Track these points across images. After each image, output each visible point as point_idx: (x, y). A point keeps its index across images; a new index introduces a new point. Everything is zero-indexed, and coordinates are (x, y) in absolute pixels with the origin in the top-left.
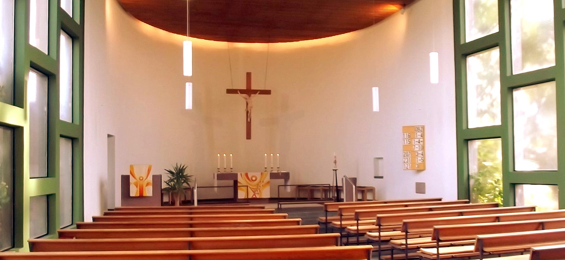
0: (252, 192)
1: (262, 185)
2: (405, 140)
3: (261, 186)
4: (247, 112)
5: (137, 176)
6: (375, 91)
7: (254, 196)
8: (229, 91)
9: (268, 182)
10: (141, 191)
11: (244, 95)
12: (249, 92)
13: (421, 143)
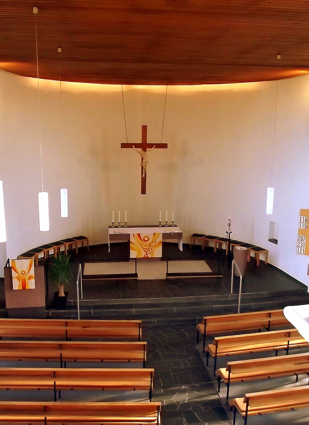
2: (302, 224)
3: (153, 246)
4: (142, 168)
6: (270, 193)
7: (146, 256)
10: (24, 285)
12: (144, 146)
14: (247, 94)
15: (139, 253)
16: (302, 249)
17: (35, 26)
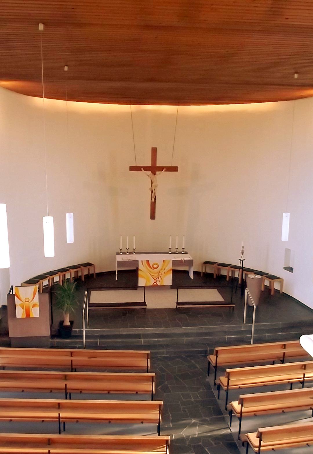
0: (154, 280)
1: (164, 273)
3: (163, 273)
4: (152, 192)
5: (22, 297)
6: (286, 219)
7: (155, 284)
8: (133, 169)
12: (154, 169)
15: (148, 280)
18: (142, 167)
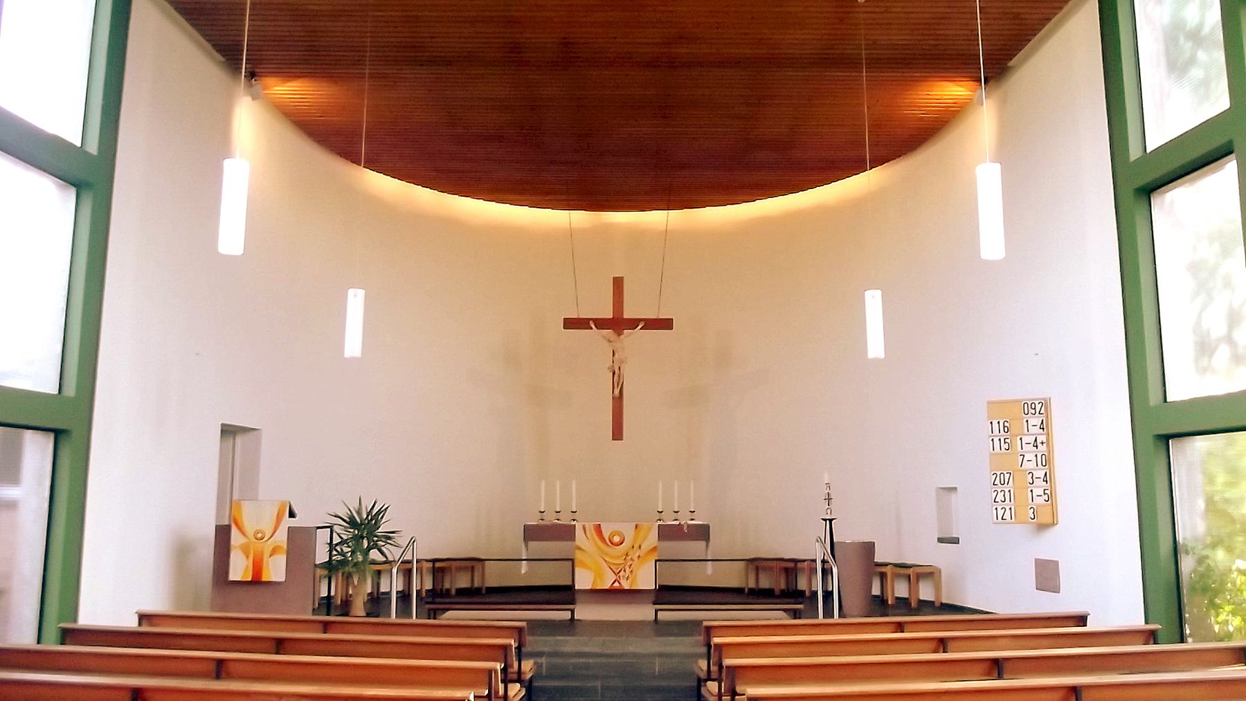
3: (636, 559)
5: (250, 527)
6: (873, 301)
7: (616, 584)
9: (654, 549)
10: (258, 568)
11: (608, 332)
12: (617, 324)
13: (1042, 448)
14: (856, 206)
15: (599, 575)
16: (1008, 508)
17: (367, 47)
18: (591, 319)
